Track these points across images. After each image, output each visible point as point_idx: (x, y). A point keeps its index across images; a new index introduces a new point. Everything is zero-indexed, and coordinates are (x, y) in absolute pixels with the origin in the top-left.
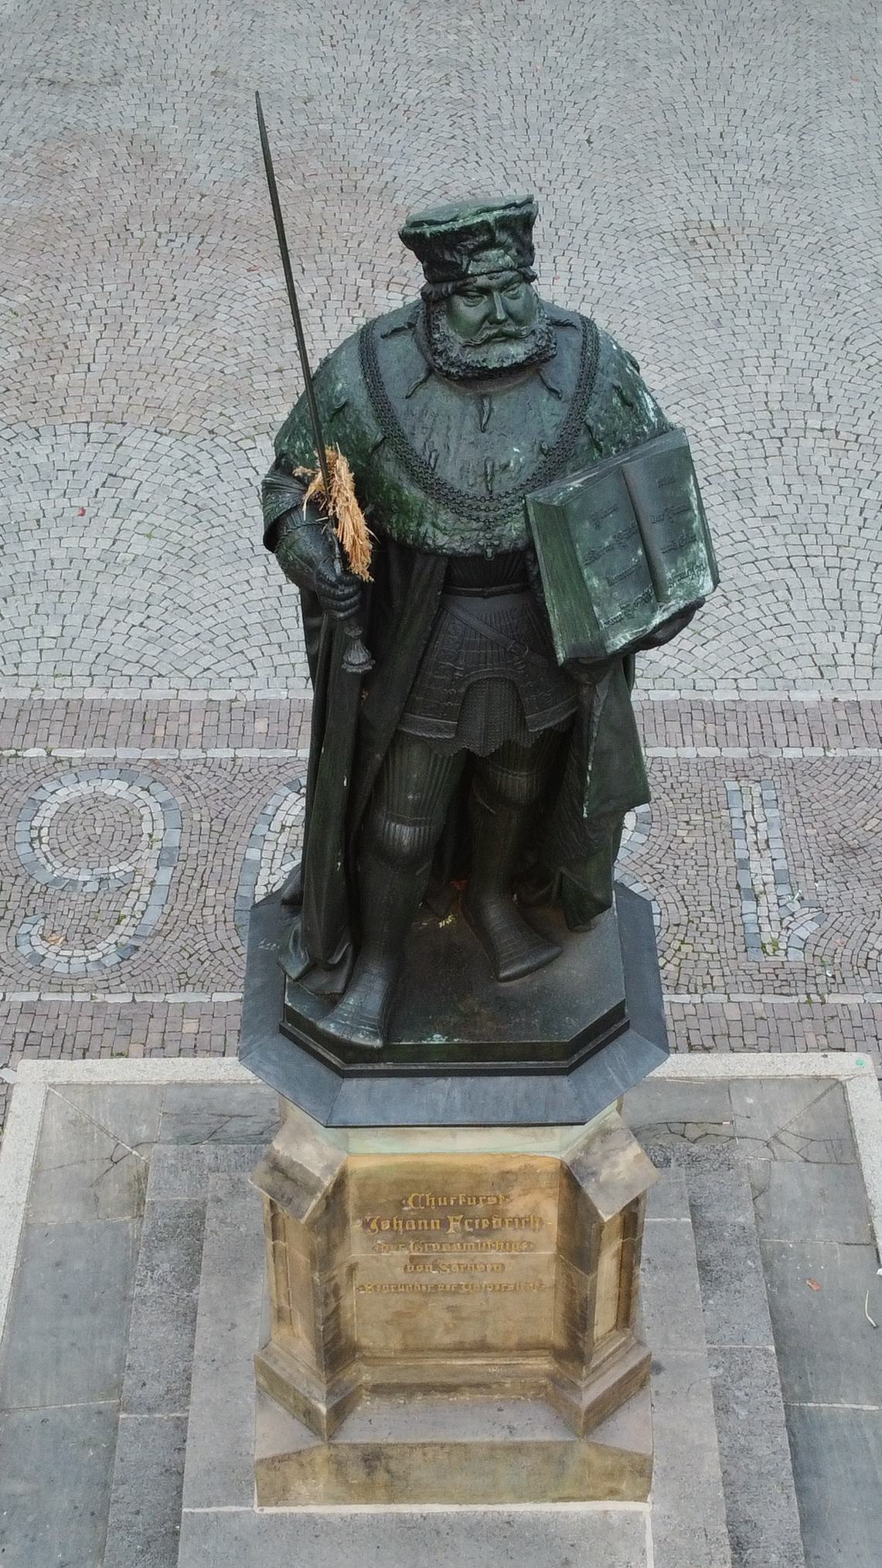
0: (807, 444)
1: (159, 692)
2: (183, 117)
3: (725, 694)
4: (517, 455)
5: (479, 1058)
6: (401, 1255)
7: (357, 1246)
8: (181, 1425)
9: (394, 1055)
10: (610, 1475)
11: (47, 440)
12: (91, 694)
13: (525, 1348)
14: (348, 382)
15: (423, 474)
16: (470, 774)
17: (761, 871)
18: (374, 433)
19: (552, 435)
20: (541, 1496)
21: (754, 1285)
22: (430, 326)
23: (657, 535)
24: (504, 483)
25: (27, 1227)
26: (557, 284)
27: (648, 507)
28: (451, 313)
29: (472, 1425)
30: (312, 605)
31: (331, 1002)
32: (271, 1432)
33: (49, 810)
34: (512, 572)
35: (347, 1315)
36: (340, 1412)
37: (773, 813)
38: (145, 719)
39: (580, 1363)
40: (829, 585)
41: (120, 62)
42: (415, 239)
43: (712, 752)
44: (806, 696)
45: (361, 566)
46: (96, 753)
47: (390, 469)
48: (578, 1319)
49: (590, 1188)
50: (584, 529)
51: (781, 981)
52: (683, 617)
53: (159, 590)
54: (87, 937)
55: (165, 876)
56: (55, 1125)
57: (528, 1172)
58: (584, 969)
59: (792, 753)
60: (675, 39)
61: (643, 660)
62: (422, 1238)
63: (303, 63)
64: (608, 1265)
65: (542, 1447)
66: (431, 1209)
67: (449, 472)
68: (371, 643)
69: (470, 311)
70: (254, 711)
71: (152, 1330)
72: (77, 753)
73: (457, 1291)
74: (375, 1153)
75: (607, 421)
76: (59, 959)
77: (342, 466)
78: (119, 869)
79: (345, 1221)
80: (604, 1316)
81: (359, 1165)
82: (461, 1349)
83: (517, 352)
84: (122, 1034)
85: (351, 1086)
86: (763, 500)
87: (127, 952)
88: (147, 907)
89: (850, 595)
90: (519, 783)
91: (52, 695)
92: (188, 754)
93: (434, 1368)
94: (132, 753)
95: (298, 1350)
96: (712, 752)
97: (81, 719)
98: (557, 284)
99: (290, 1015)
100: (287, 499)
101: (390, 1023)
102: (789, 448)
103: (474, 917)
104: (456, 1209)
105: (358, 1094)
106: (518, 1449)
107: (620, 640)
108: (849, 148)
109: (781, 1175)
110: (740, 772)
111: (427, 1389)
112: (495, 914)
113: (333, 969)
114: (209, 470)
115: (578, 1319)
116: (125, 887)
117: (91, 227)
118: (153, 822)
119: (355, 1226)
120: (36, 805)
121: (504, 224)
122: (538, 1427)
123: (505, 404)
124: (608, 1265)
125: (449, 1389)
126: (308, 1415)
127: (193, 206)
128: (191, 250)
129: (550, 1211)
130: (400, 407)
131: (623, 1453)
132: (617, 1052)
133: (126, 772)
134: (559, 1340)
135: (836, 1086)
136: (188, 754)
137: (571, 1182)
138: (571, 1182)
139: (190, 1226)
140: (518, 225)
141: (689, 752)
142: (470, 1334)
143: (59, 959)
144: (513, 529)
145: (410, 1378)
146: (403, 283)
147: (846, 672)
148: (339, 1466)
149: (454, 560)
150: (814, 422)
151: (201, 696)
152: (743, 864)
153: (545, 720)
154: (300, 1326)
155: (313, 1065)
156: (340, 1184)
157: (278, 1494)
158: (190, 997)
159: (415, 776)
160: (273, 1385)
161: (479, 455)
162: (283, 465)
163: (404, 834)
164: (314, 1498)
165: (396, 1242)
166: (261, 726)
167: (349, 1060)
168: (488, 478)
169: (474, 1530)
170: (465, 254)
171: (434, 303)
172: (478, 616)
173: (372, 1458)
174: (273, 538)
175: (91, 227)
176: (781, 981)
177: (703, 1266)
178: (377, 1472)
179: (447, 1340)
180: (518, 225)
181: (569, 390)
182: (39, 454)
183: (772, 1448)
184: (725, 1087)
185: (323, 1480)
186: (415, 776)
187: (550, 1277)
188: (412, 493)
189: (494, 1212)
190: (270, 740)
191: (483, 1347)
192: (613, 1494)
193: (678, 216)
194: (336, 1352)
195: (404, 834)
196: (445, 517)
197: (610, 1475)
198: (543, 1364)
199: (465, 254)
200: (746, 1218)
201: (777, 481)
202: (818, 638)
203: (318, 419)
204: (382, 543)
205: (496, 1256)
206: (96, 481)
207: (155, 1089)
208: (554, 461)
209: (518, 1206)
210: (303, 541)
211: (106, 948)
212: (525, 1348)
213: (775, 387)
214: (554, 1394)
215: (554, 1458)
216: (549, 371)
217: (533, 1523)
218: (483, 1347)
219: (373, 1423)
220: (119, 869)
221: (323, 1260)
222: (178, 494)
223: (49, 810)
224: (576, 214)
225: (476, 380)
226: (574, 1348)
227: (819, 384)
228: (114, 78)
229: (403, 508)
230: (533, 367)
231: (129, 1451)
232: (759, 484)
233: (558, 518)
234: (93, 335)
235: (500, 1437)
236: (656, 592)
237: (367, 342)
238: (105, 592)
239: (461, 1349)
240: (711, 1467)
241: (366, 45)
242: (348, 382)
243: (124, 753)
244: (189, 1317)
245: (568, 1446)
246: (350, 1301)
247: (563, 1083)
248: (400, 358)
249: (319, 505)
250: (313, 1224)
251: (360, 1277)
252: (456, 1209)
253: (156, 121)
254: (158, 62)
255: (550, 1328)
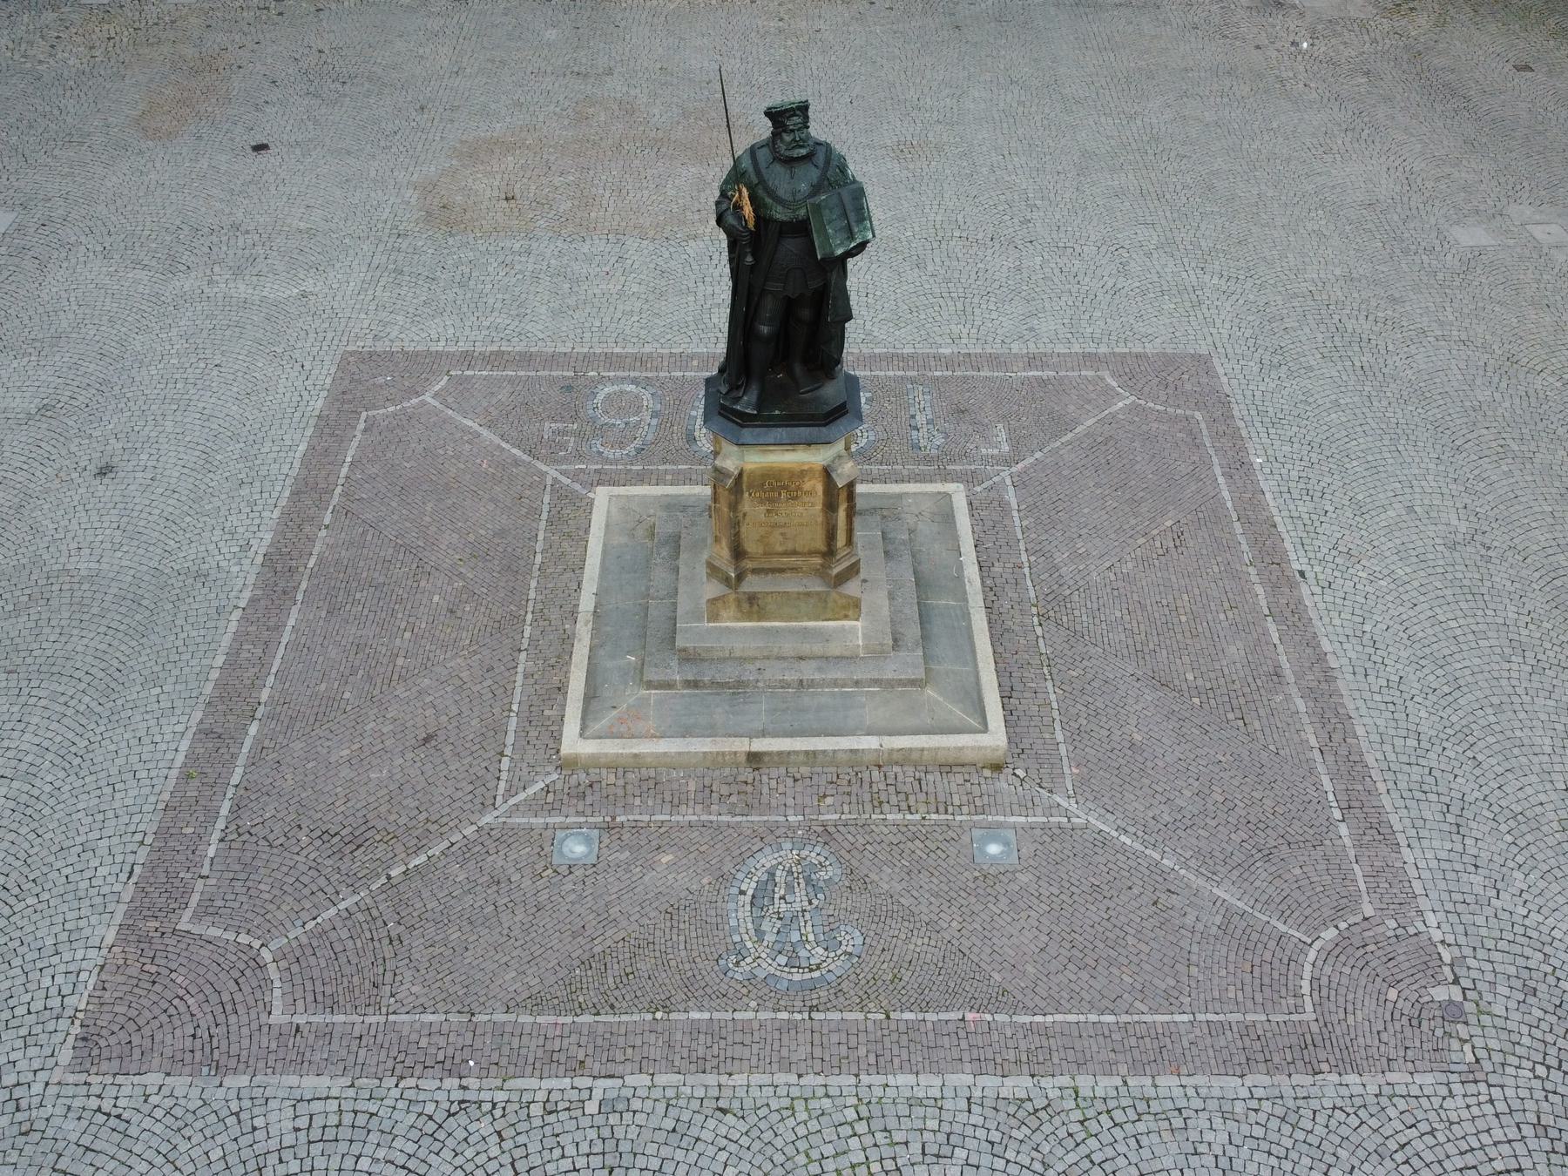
0: (952, 243)
1: (648, 349)
2: (646, 91)
3: (908, 350)
4: (804, 187)
5: (791, 420)
6: (763, 508)
7: (747, 505)
8: (675, 604)
9: (759, 419)
10: (844, 607)
11: (588, 242)
12: (617, 350)
13: (811, 553)
14: (746, 164)
15: (771, 193)
16: (789, 307)
17: (920, 419)
18: (755, 181)
19: (815, 181)
20: (817, 619)
21: (907, 558)
22: (774, 143)
23: (852, 217)
24: (799, 197)
25: (605, 545)
26: (816, 131)
27: (849, 207)
28: (782, 140)
29: (791, 584)
30: (732, 246)
31: (737, 400)
32: (713, 589)
33: (601, 396)
34: (801, 228)
35: (743, 535)
36: (740, 577)
37: (928, 397)
38: (642, 361)
39: (832, 563)
40: (960, 305)
41: (612, 64)
42: (769, 114)
43: (901, 373)
44: (946, 351)
45: (751, 225)
46: (620, 374)
47: (761, 192)
48: (831, 536)
49: (834, 475)
50: (826, 212)
51: (928, 460)
52: (862, 246)
53: (645, 307)
54: (622, 445)
55: (654, 422)
56: (614, 510)
57: (811, 470)
58: (831, 392)
59: (938, 374)
60: (897, 51)
61: (851, 262)
62: (771, 500)
63: (706, 64)
64: (842, 514)
65: (818, 593)
66: (777, 486)
67: (781, 193)
68: (753, 255)
69: (787, 138)
70: (692, 357)
71: (660, 575)
72: (612, 374)
73: (784, 525)
74: (757, 460)
75: (831, 173)
76: (609, 453)
77: (744, 190)
78: (634, 419)
79: (742, 493)
80: (841, 539)
81: (748, 467)
82: (786, 554)
83: (803, 152)
84: (641, 479)
85: (746, 431)
86: (930, 268)
87: (639, 451)
88: (647, 432)
89: (969, 310)
90: (806, 313)
91: (598, 351)
92: (662, 374)
93: (776, 562)
94: (637, 374)
95: (724, 552)
96: (901, 373)
97: (611, 360)
98: (816, 131)
99: (723, 407)
100: (724, 206)
101: (760, 406)
102: (944, 245)
103: (790, 373)
104: (783, 487)
105: (747, 434)
106: (808, 594)
107: (839, 252)
108: (983, 106)
109: (921, 526)
110: (913, 381)
111: (773, 571)
112: (798, 369)
113: (738, 388)
114: (666, 255)
115: (831, 536)
116: (637, 425)
117: (603, 144)
118: (646, 396)
119: (746, 495)
120: (595, 395)
121: (799, 108)
122: (817, 586)
123: (800, 170)
124: (842, 514)
125: (782, 571)
126: (726, 580)
127: (653, 134)
128: (653, 154)
129: (820, 488)
130: (763, 171)
131: (850, 597)
132: (843, 420)
133: (635, 381)
134: (823, 548)
135: (947, 495)
136: (662, 374)
137: (827, 473)
138: (827, 473)
139: (675, 542)
140: (803, 109)
141: (891, 373)
142: (790, 546)
143: (609, 453)
144: (802, 212)
145: (766, 566)
146: (765, 129)
147: (964, 341)
148: (738, 602)
149: (783, 223)
150: (957, 234)
151: (666, 351)
152: (913, 417)
153: (815, 284)
154: (724, 543)
155: (731, 425)
156: (741, 474)
157: (714, 617)
158: (668, 467)
159: (769, 307)
160: (713, 570)
161: (791, 185)
162: (723, 194)
163: (765, 329)
164: (729, 619)
165: (762, 502)
166: (695, 363)
167: (744, 420)
168: (794, 194)
169: (792, 631)
170: (787, 119)
171: (776, 135)
172: (791, 246)
173: (752, 598)
174: (719, 221)
175: (603, 144)
176: (928, 460)
177: (886, 552)
178: (753, 606)
179: (780, 549)
180: (803, 109)
181: (821, 165)
182: (585, 248)
183: (912, 611)
184: (900, 496)
185: (732, 611)
186: (769, 307)
187: (820, 519)
188: (769, 201)
189: (799, 488)
190: (699, 369)
191: (794, 553)
192: (846, 617)
193: (895, 139)
194: (738, 553)
195: (765, 329)
196: (779, 208)
197: (844, 607)
198: (818, 560)
199: (787, 119)
200: (905, 537)
201: (937, 260)
202: (953, 327)
203: (736, 176)
204: (758, 218)
205: (800, 509)
206: (613, 260)
207: (656, 497)
208: (816, 189)
209: (807, 486)
210: (731, 220)
211: (630, 449)
212: (811, 553)
213: (939, 218)
214: (822, 573)
215: (822, 598)
216: (815, 159)
217: (814, 629)
218: (794, 553)
219: (752, 584)
220: (634, 419)
221: (734, 507)
222: (652, 266)
223: (601, 396)
224: (844, 137)
225: (790, 162)
226: (830, 553)
227: (960, 218)
228: (610, 72)
229: (765, 205)
230: (808, 157)
231: (653, 612)
232: (929, 262)
233: (818, 208)
234: (607, 195)
235: (801, 589)
236: (851, 237)
237: (753, 151)
238: (620, 307)
239: (786, 554)
240: (885, 611)
241: (738, 55)
242: (746, 164)
243: (632, 374)
244: (676, 570)
245: (828, 593)
246: (743, 529)
247: (823, 429)
248: (764, 156)
249: (738, 207)
250: (730, 490)
251: (748, 519)
252: (783, 487)
253: (632, 92)
254: (632, 64)
255: (820, 545)
